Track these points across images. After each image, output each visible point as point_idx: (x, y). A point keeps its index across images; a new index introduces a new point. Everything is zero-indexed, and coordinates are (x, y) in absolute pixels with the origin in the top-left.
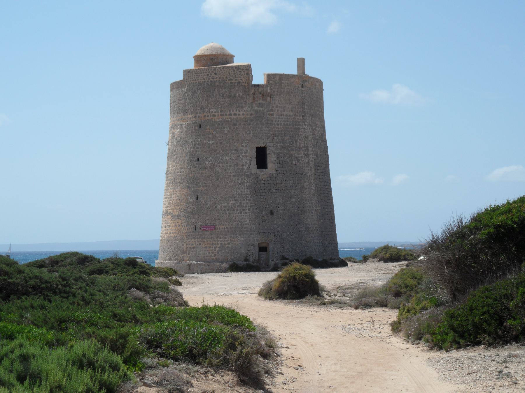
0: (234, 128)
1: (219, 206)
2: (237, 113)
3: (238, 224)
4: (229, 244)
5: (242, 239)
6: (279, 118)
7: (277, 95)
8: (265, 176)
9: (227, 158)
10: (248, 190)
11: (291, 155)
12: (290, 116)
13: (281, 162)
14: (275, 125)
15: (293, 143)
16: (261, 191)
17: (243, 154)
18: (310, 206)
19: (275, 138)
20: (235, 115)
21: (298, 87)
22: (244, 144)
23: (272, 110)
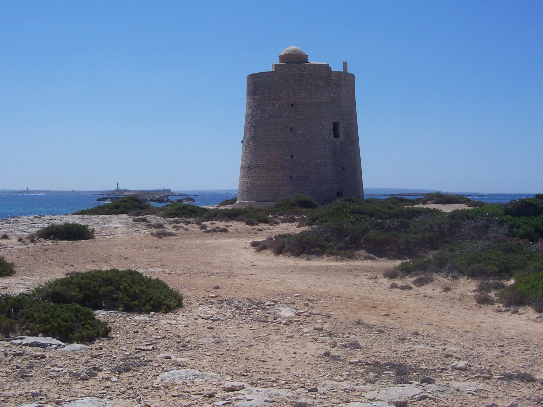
1: (310, 163)
2: (321, 97)
20: (319, 99)
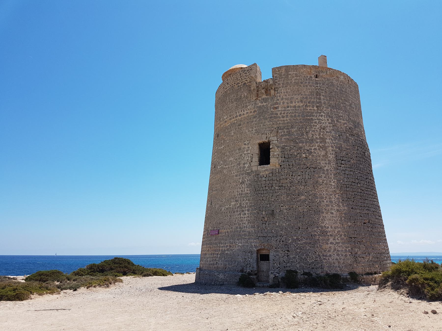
0: (239, 128)
2: (242, 113)
3: (237, 227)
4: (228, 250)
5: (240, 244)
6: (284, 110)
7: (283, 87)
8: (267, 173)
9: (232, 159)
10: (248, 189)
11: (301, 148)
12: (299, 107)
13: (286, 156)
14: (279, 118)
15: (303, 134)
16: (261, 189)
17: (245, 152)
18: (328, 205)
19: (280, 131)
21: (311, 77)
22: (246, 142)
23: (277, 103)
